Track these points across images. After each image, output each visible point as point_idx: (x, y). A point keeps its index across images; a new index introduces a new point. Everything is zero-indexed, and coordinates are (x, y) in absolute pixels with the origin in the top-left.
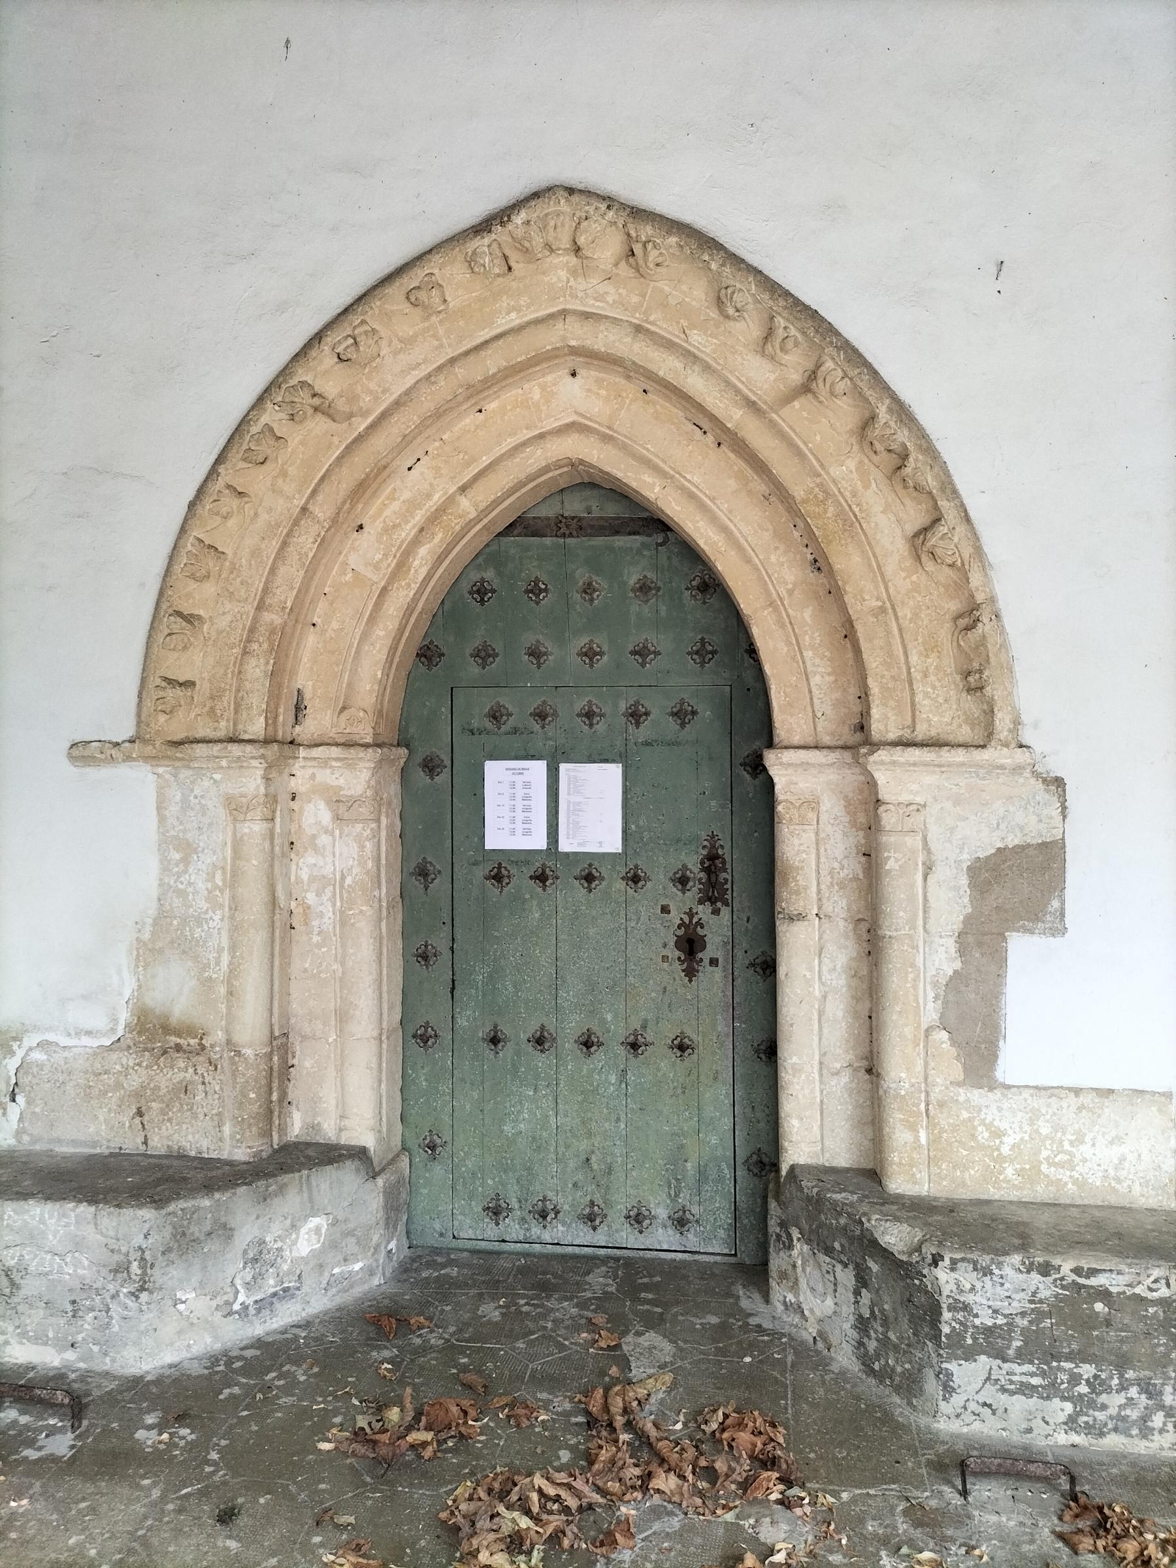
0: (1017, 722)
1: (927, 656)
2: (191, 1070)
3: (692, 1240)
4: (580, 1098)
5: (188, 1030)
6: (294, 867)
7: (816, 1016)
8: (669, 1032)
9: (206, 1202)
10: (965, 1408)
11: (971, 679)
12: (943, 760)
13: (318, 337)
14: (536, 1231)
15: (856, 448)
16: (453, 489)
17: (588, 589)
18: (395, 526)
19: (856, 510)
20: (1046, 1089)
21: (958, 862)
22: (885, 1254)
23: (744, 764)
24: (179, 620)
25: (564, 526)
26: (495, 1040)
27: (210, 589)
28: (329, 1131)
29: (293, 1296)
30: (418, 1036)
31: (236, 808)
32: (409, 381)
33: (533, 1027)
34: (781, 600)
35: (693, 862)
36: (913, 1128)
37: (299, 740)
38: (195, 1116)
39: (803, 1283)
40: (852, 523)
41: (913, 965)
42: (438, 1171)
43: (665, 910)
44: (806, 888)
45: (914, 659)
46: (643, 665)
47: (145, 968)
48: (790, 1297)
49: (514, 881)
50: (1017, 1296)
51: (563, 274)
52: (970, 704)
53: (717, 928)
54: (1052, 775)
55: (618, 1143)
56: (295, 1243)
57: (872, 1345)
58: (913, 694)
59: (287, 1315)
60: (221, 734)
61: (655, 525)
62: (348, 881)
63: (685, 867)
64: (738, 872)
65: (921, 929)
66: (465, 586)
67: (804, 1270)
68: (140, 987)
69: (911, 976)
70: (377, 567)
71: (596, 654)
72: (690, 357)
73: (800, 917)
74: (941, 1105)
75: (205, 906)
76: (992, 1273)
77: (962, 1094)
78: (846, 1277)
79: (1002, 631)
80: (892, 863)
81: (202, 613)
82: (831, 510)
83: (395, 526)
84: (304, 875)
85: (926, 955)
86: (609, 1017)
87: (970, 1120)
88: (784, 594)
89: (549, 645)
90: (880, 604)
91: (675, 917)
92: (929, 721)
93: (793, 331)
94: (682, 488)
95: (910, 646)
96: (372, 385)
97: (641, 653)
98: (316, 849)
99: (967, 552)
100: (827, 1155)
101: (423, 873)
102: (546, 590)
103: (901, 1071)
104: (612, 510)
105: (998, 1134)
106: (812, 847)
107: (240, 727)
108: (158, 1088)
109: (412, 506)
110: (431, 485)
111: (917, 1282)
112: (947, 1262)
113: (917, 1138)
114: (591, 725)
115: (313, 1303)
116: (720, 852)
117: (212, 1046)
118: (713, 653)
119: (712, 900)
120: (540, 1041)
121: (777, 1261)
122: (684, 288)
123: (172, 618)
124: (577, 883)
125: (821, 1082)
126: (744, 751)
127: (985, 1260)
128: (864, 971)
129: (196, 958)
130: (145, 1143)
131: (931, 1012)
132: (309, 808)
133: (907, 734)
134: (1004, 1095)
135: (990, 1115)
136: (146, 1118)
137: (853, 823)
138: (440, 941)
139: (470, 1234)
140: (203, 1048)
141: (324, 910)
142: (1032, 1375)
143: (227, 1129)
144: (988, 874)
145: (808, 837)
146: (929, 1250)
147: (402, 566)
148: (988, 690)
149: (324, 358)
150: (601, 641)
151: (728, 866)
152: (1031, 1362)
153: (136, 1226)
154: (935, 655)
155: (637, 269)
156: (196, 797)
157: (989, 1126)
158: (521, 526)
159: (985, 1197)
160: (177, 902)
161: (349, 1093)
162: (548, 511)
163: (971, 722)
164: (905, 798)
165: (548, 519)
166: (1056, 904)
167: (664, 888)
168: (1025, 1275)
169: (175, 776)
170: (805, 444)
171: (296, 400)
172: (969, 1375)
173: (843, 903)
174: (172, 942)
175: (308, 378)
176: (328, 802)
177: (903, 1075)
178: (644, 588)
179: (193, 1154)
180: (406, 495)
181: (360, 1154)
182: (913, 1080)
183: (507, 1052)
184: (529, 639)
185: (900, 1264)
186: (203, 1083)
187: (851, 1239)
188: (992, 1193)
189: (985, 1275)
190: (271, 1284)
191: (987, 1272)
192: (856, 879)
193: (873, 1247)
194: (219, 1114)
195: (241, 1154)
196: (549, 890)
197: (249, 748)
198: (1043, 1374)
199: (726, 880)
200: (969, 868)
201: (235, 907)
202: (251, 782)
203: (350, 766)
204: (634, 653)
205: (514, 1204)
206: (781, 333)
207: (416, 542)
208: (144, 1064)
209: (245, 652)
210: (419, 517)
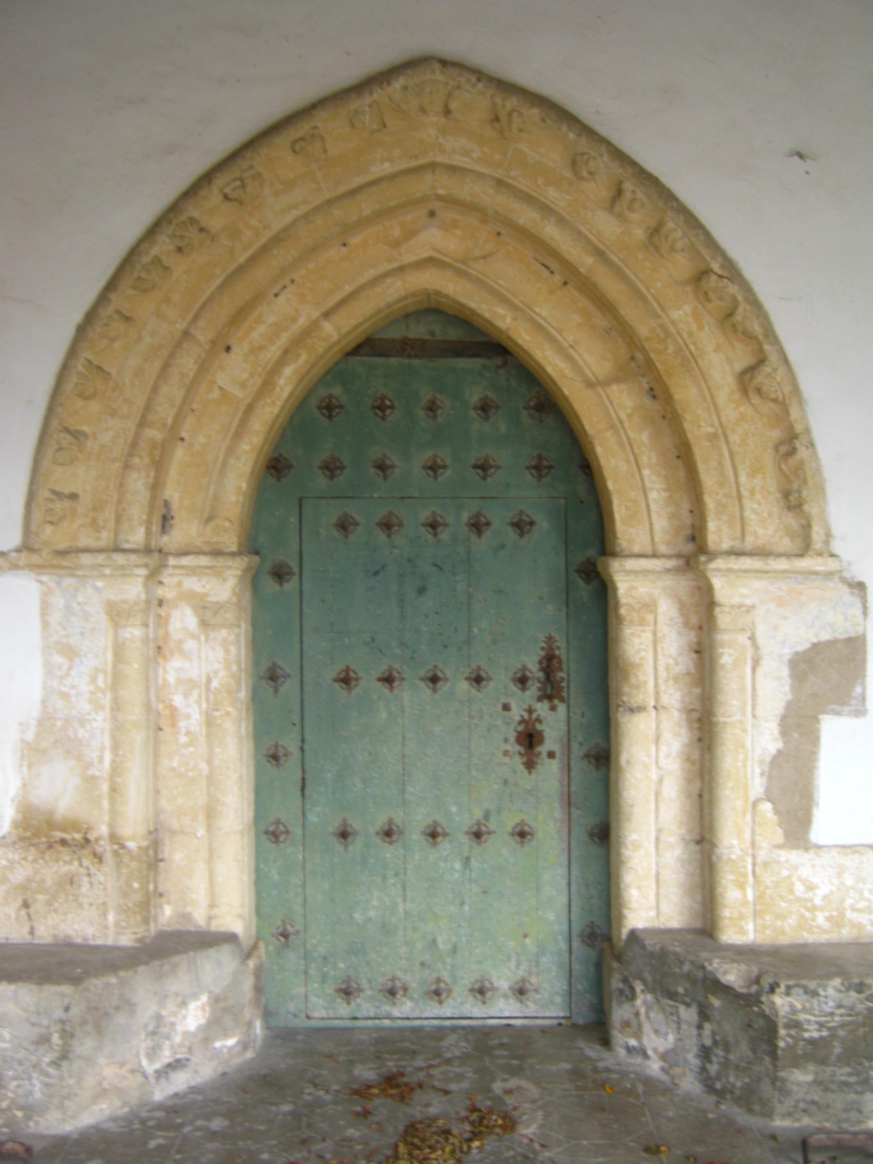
0: (828, 535)
1: (754, 477)
2: (76, 863)
3: (531, 1009)
4: (426, 885)
5: (72, 825)
6: (161, 671)
7: (652, 798)
8: (511, 821)
9: (113, 980)
10: (796, 1107)
11: (791, 498)
12: (769, 568)
13: (207, 178)
14: (387, 1008)
15: (691, 296)
16: (316, 314)
17: (432, 408)
18: (262, 348)
19: (692, 348)
20: (849, 847)
21: (781, 656)
22: (725, 990)
23: (578, 571)
24: (68, 436)
25: (407, 348)
26: (344, 835)
27: (95, 406)
28: (200, 917)
29: (184, 1066)
30: (270, 833)
31: (117, 614)
32: (288, 219)
33: (381, 822)
34: (621, 422)
35: (532, 662)
36: (742, 886)
37: (166, 549)
38: (80, 906)
39: (646, 1027)
40: (689, 361)
41: (743, 746)
42: (292, 958)
43: (506, 707)
44: (645, 683)
45: (743, 479)
46: (484, 478)
47: (30, 767)
48: (633, 1042)
49: (362, 683)
50: (838, 1012)
51: (432, 132)
52: (791, 521)
53: (554, 723)
54: (856, 580)
55: (463, 924)
56: (184, 1018)
57: (713, 1069)
58: (742, 509)
59: (181, 1081)
60: (102, 543)
61: (495, 349)
62: (215, 684)
63: (524, 668)
64: (572, 672)
65: (749, 715)
66: (314, 402)
67: (648, 1017)
68: (25, 785)
69: (741, 756)
70: (243, 385)
71: (440, 467)
72: (546, 210)
73: (641, 709)
74: (766, 865)
75: (88, 707)
76: (818, 995)
77: (783, 855)
78: (689, 1014)
79: (817, 459)
80: (726, 658)
81: (86, 428)
82: (671, 349)
83: (262, 348)
84: (171, 678)
85: (753, 738)
86: (454, 809)
87: (789, 877)
88: (623, 417)
89: (394, 459)
90: (712, 430)
91: (517, 713)
92: (755, 533)
93: (640, 195)
94: (532, 320)
95: (740, 467)
96: (254, 222)
97: (483, 467)
98: (182, 652)
99: (787, 389)
100: (662, 919)
101: (273, 676)
102: (392, 407)
103: (732, 840)
104: (453, 334)
105: (811, 887)
106: (652, 646)
107: (122, 537)
108: (43, 881)
109: (278, 329)
110: (297, 310)
111: (755, 1009)
112: (782, 988)
113: (745, 896)
114: (435, 535)
115: (201, 1072)
116: (557, 652)
117: (97, 840)
118: (550, 468)
119: (550, 698)
120: (388, 833)
121: (619, 1013)
122: (542, 150)
123: (62, 435)
124: (422, 684)
125: (658, 855)
126: (579, 558)
127: (812, 985)
128: (696, 755)
129: (79, 758)
130: (32, 932)
131: (757, 786)
132: (176, 614)
133: (737, 544)
134: (817, 854)
135: (805, 872)
136: (32, 910)
137: (686, 624)
138: (291, 743)
139: (324, 1014)
140: (87, 841)
141: (192, 712)
142: (850, 1075)
143: (111, 917)
144: (804, 665)
145: (647, 636)
146: (766, 981)
147: (267, 385)
148: (806, 508)
149: (213, 196)
150: (445, 454)
151: (564, 666)
152: (848, 1064)
153: (53, 997)
154: (759, 476)
155: (501, 133)
156: (79, 604)
157: (804, 881)
158: (368, 346)
159: (801, 941)
160: (60, 704)
161: (217, 883)
162: (395, 333)
163: (790, 533)
164: (736, 600)
165: (393, 340)
166: (858, 690)
167: (506, 687)
168: (844, 994)
169: (59, 584)
170: (648, 289)
171: (185, 234)
172: (800, 1077)
173: (677, 696)
174: (56, 742)
175: (196, 215)
176: (195, 609)
177: (735, 842)
178: (485, 408)
179: (79, 941)
180: (272, 319)
181: (230, 938)
182: (743, 846)
183: (356, 846)
184: (376, 452)
185: (738, 996)
186: (89, 875)
187: (694, 982)
188: (807, 937)
189: (813, 997)
190: (166, 1056)
191: (815, 994)
192: (688, 673)
193: (716, 986)
194: (104, 904)
195: (126, 940)
196: (396, 691)
197: (133, 557)
198: (858, 1074)
199: (562, 679)
200: (790, 661)
201: (117, 707)
202: (133, 589)
203: (218, 573)
204: (475, 467)
205: (365, 984)
206: (628, 196)
207: (281, 363)
208: (30, 858)
209: (127, 466)
210: (284, 339)
